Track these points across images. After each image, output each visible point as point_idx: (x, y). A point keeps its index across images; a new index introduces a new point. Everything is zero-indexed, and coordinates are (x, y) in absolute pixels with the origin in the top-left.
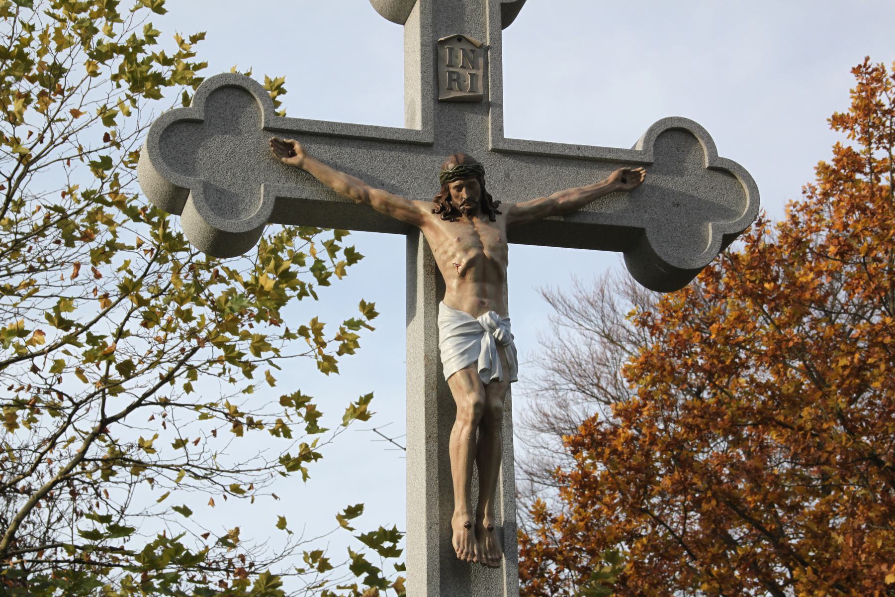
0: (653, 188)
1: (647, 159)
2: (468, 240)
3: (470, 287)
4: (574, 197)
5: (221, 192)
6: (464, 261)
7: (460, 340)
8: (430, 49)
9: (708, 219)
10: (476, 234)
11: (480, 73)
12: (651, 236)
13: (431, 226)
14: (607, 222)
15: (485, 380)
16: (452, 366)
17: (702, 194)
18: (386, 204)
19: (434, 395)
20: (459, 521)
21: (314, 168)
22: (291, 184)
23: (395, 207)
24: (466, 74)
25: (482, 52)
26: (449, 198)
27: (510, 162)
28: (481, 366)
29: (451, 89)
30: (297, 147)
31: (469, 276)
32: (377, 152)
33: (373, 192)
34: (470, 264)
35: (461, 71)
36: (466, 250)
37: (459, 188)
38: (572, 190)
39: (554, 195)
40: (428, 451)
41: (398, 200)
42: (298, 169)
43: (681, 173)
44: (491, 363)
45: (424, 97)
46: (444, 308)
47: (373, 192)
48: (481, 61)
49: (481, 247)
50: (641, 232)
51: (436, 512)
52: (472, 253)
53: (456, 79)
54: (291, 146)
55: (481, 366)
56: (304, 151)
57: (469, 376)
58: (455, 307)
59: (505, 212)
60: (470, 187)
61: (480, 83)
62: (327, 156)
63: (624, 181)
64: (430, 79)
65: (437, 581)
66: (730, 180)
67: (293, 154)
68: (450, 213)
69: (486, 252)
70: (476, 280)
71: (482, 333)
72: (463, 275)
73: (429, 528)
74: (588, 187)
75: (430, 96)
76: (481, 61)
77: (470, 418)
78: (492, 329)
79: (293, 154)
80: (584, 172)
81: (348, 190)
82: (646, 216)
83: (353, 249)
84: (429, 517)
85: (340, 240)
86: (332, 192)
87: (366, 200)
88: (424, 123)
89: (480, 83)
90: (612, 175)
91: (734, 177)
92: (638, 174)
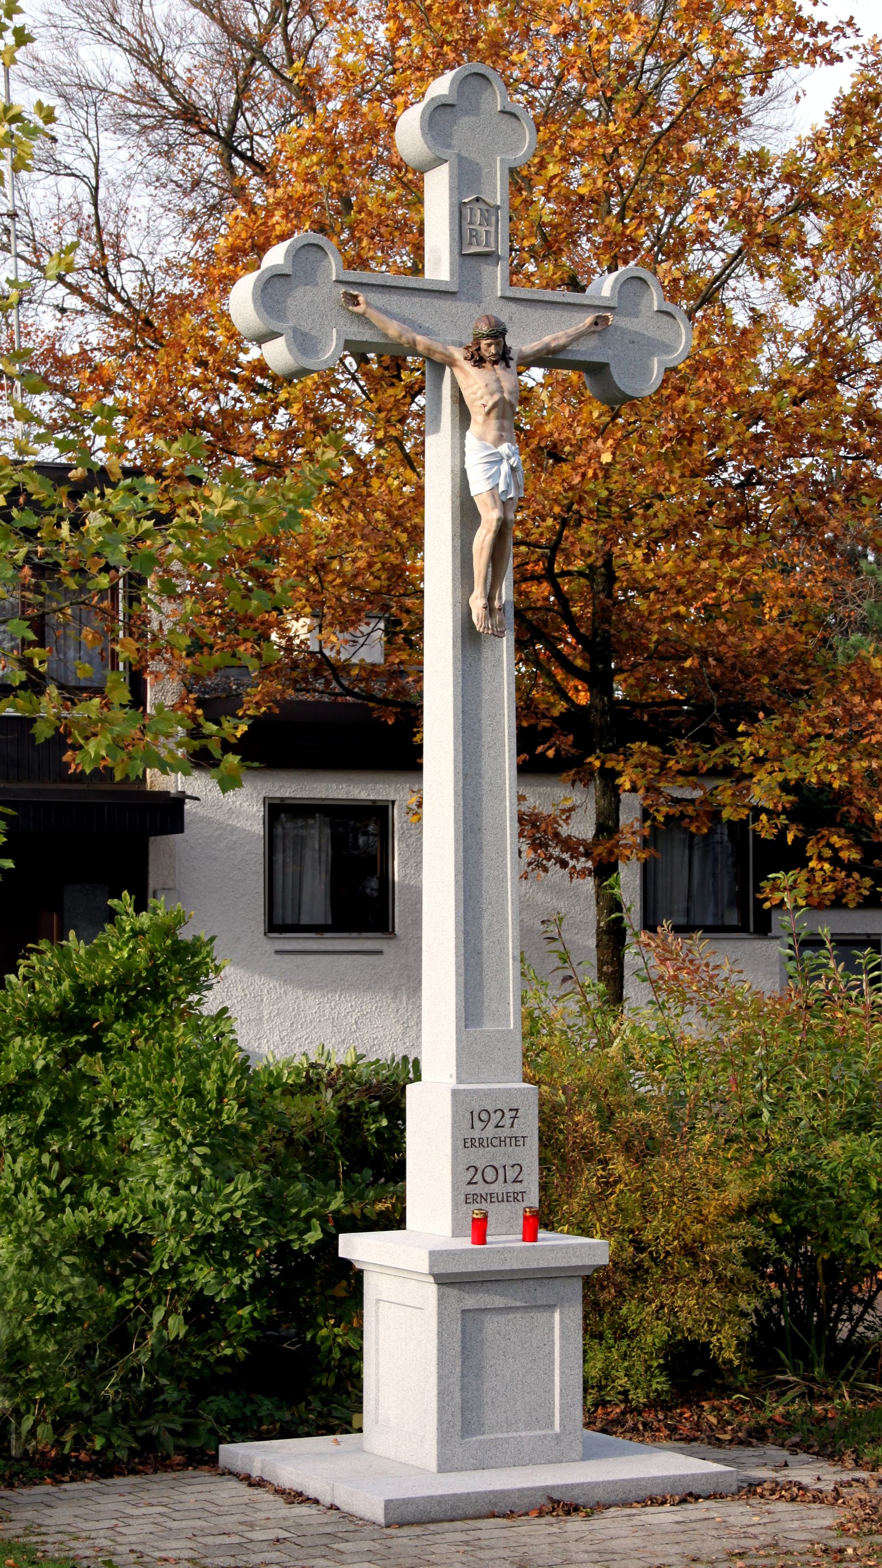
0: (616, 328)
1: (613, 304)
2: (493, 386)
3: (493, 423)
4: (562, 341)
5: (305, 335)
6: (490, 404)
7: (486, 466)
8: (456, 209)
9: (653, 354)
10: (498, 380)
11: (492, 229)
12: (613, 369)
13: (462, 369)
14: (582, 359)
15: (503, 498)
16: (479, 487)
17: (650, 333)
18: (429, 349)
19: (458, 501)
20: (477, 603)
21: (375, 316)
22: (354, 328)
23: (435, 352)
24: (482, 230)
25: (492, 211)
26: (479, 349)
27: (513, 306)
28: (502, 488)
29: (471, 244)
30: (361, 299)
31: (493, 414)
32: (416, 299)
33: (419, 338)
34: (495, 405)
35: (478, 228)
36: (492, 394)
37: (489, 345)
38: (560, 334)
39: (547, 339)
40: (453, 546)
41: (438, 347)
42: (361, 316)
43: (636, 315)
44: (508, 486)
45: (451, 252)
46: (471, 436)
47: (419, 338)
48: (493, 219)
49: (501, 390)
50: (606, 365)
51: (459, 593)
52: (496, 397)
53: (474, 234)
54: (356, 297)
55: (502, 488)
56: (368, 304)
57: (493, 496)
58: (481, 438)
59: (515, 357)
60: (497, 344)
61: (492, 239)
62: (379, 304)
63: (596, 324)
64: (457, 236)
65: (459, 645)
66: (671, 320)
67: (358, 304)
68: (479, 361)
69: (506, 395)
70: (498, 418)
71: (501, 460)
72: (488, 413)
73: (454, 605)
74: (572, 331)
75: (457, 250)
76: (493, 219)
77: (493, 528)
78: (509, 458)
79: (358, 304)
80: (566, 315)
81: (400, 336)
82: (610, 352)
83: (23, 28)
84: (454, 598)
85: (10, 18)
86: (386, 335)
87: (414, 343)
88: (452, 275)
89: (492, 239)
90: (589, 319)
91: (673, 317)
92: (606, 319)
